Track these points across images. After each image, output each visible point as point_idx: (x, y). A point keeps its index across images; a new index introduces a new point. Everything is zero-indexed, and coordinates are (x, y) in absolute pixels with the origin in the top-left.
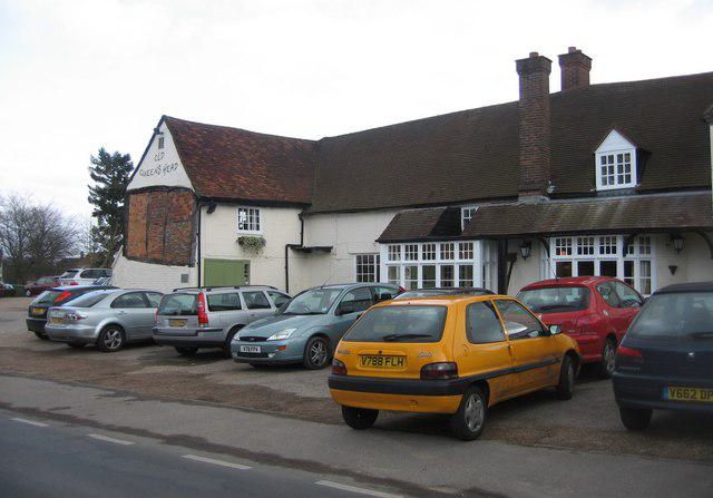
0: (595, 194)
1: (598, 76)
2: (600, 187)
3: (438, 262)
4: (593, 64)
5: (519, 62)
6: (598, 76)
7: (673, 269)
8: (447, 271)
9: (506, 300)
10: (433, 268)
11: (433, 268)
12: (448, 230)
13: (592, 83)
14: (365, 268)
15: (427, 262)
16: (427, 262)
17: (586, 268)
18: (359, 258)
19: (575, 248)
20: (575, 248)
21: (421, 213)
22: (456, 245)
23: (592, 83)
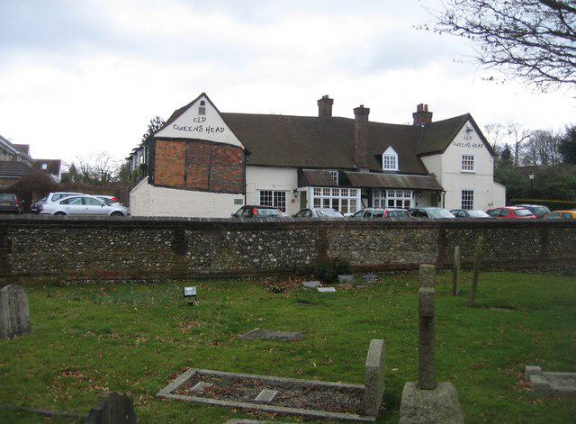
0: (382, 172)
1: (372, 118)
2: (384, 169)
3: (340, 197)
4: (334, 101)
5: (362, 106)
6: (372, 118)
7: (416, 204)
8: (345, 202)
9: (37, 222)
10: (346, 200)
11: (346, 200)
12: (345, 183)
13: (333, 115)
14: (266, 199)
15: (344, 197)
16: (344, 197)
17: (399, 203)
18: (262, 193)
19: (395, 194)
20: (395, 194)
21: (318, 172)
22: (349, 190)
23: (333, 115)
